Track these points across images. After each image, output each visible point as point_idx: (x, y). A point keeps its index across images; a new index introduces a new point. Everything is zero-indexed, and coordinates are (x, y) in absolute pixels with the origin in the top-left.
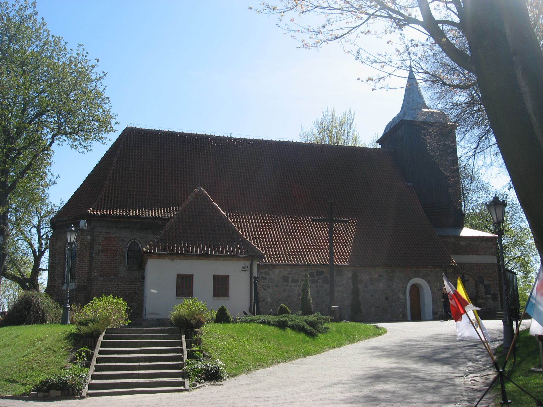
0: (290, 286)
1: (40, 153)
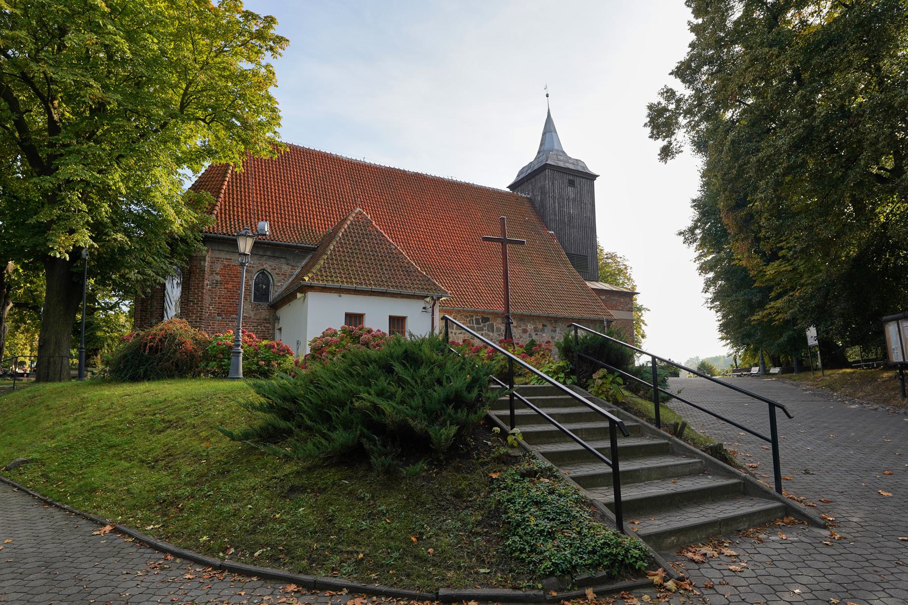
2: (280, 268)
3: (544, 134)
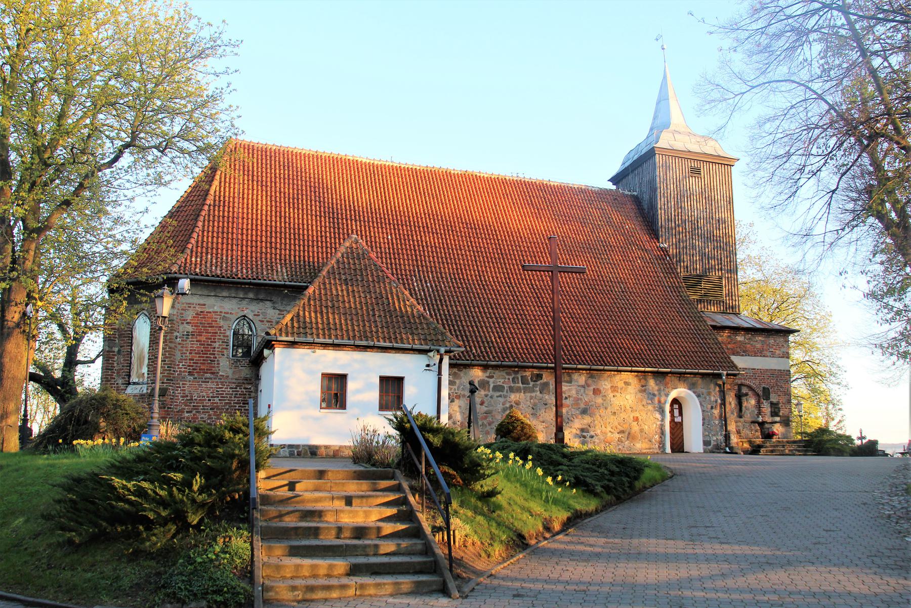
0: (491, 397)
1: (88, 189)
2: (264, 314)
3: (658, 103)
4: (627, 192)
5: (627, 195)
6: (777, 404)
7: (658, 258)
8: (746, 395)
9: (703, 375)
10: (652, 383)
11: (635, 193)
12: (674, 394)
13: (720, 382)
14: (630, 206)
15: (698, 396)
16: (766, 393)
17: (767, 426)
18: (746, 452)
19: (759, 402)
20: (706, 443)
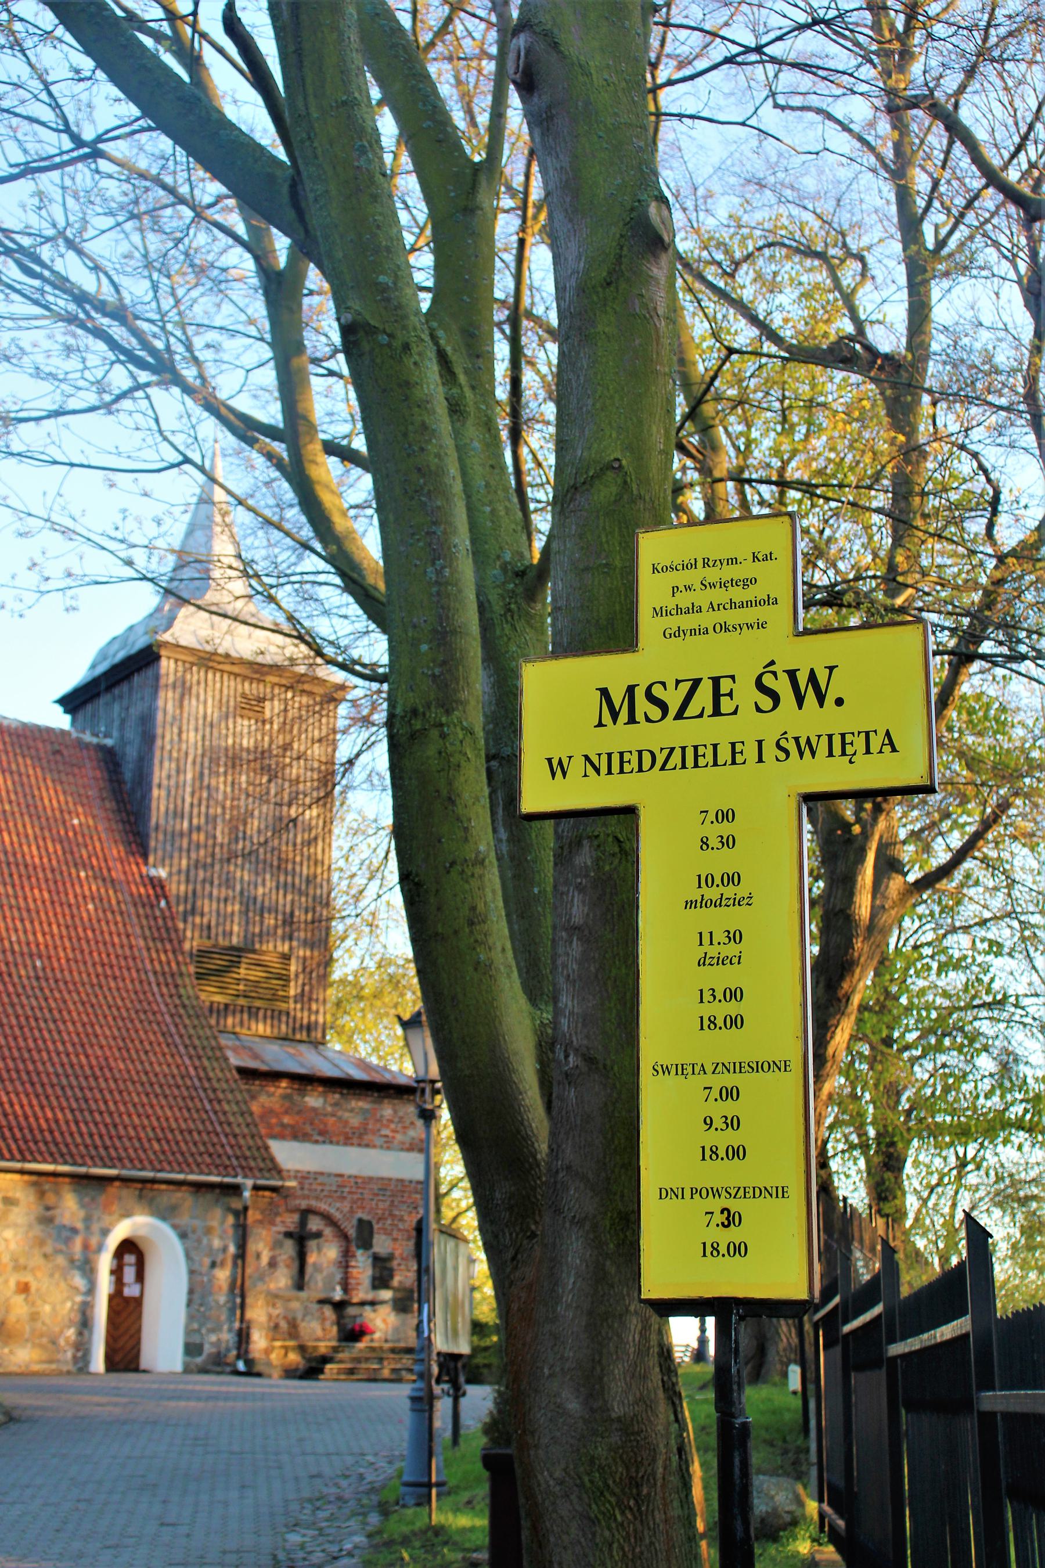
4: (88, 738)
5: (87, 746)
6: (390, 1258)
7: (137, 902)
8: (318, 1235)
9: (199, 1187)
10: (70, 1206)
11: (109, 742)
12: (121, 1231)
13: (236, 1204)
14: (92, 773)
15: (183, 1236)
16: (365, 1234)
17: (351, 1311)
18: (290, 1373)
19: (347, 1255)
20: (191, 1349)
